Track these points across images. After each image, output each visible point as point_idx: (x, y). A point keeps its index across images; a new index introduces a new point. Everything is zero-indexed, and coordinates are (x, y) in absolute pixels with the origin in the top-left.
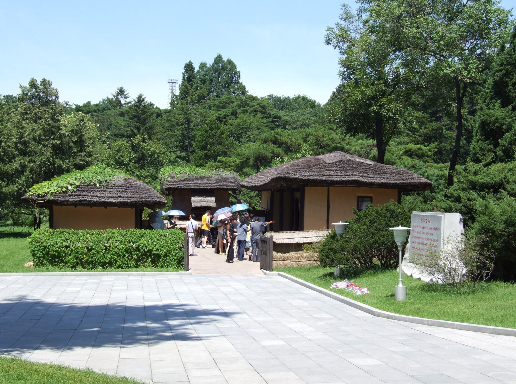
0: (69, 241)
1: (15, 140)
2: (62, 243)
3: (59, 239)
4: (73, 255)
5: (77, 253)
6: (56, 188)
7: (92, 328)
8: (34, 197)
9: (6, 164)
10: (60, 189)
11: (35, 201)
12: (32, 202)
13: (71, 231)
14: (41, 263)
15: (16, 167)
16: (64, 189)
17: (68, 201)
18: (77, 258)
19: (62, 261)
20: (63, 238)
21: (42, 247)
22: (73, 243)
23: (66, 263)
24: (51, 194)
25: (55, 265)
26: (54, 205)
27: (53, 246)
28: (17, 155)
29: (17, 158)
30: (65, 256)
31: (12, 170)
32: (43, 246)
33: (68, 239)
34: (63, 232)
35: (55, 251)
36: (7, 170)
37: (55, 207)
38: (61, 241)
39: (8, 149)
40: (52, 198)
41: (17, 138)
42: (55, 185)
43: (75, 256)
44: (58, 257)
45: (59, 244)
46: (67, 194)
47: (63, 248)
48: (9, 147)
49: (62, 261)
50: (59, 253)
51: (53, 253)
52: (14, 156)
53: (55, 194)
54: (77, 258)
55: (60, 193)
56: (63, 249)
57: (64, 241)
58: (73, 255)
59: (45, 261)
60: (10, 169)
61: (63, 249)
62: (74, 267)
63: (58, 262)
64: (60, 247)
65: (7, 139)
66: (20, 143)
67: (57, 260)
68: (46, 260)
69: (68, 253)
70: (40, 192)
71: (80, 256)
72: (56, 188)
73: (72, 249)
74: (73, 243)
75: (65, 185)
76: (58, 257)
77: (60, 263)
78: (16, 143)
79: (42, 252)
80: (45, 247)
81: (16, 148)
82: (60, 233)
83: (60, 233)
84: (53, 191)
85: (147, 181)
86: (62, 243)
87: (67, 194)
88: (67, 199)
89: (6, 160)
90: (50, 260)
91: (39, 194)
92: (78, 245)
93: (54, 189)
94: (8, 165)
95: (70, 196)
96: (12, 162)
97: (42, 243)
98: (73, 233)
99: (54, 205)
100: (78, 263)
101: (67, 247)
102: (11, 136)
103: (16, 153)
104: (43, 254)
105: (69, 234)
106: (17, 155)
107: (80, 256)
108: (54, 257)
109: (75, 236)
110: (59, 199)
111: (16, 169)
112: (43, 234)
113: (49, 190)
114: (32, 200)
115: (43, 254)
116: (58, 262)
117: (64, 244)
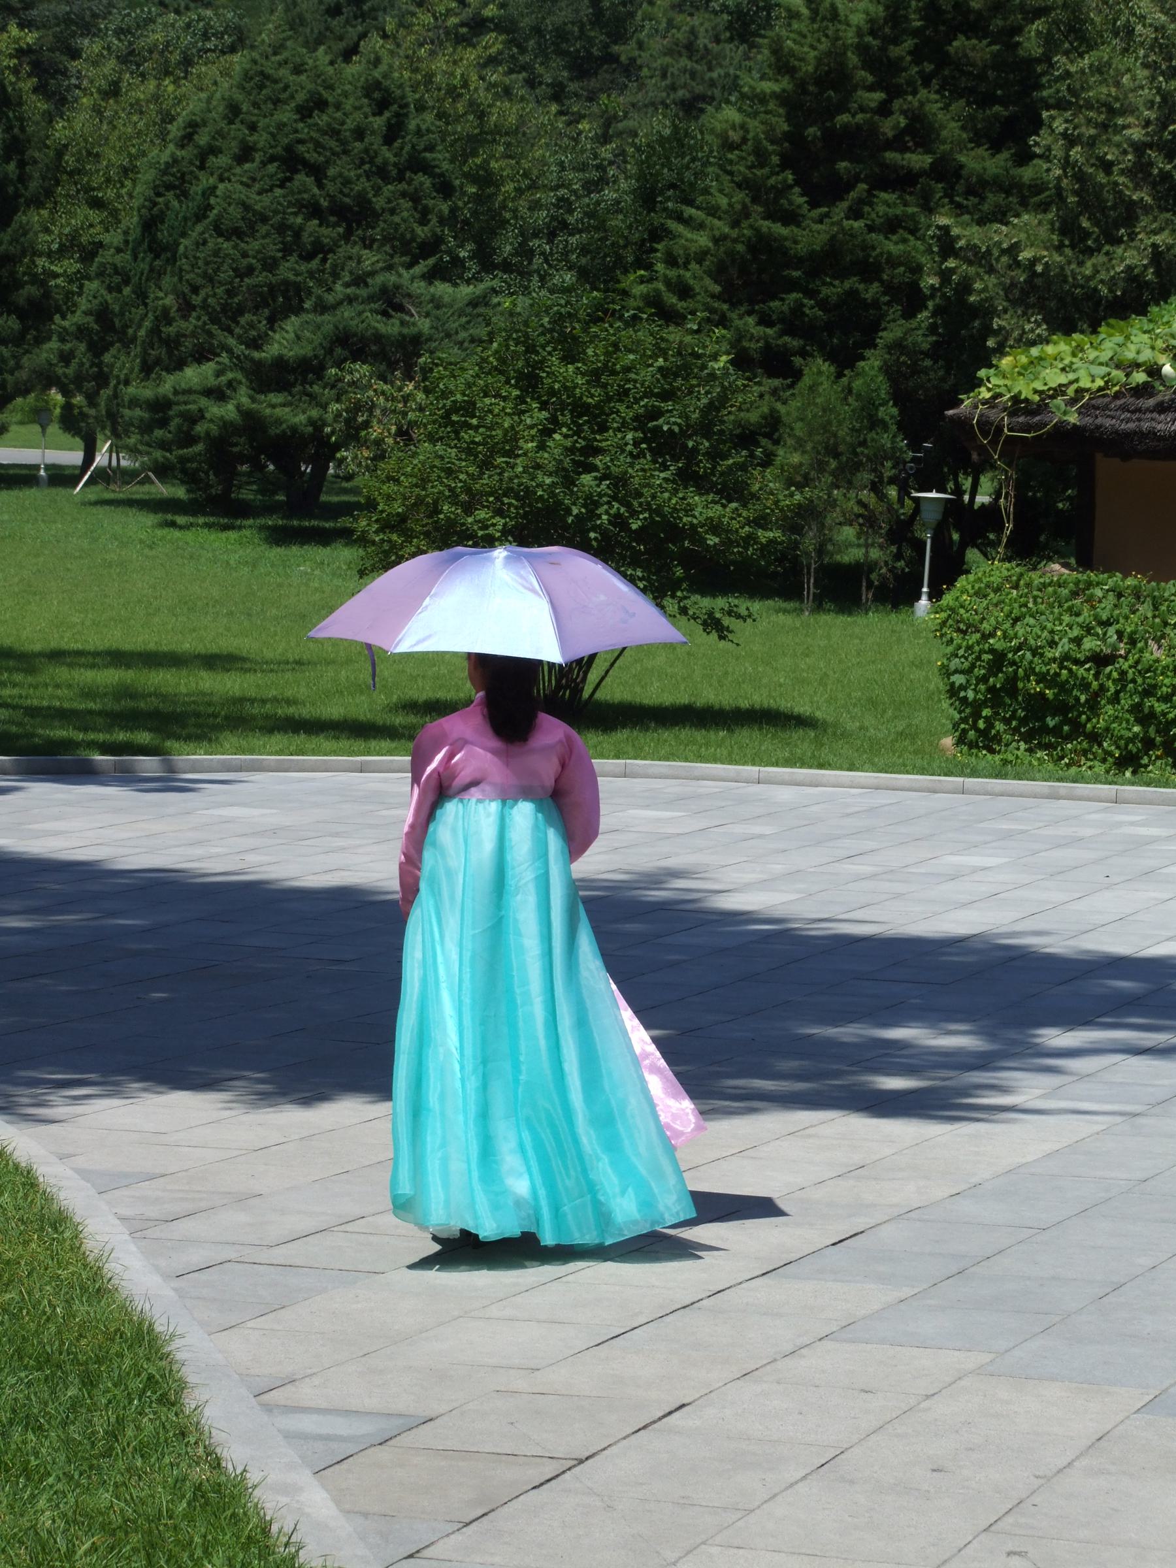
0: (1111, 631)
1: (1136, 134)
2: (1078, 641)
3: (1066, 618)
4: (1126, 702)
5: (1149, 692)
6: (1104, 370)
7: (834, 1023)
8: (994, 415)
9: (1090, 252)
10: (1118, 374)
11: (999, 429)
12: (985, 434)
13: (1130, 582)
14: (984, 733)
15: (1129, 268)
16: (1140, 377)
17: (1152, 433)
18: (1146, 718)
19: (1078, 729)
20: (1086, 616)
21: (986, 657)
22: (1133, 642)
23: (1095, 738)
24: (1073, 402)
25: (1041, 746)
26: (1099, 456)
27: (1035, 652)
28: (1147, 209)
29: (1144, 221)
30: (1093, 706)
31: (1112, 283)
32: (992, 651)
33: (1107, 624)
34: (1089, 584)
35: (1042, 678)
36: (1089, 279)
37: (1105, 465)
38: (1076, 632)
39: (1101, 178)
40: (1073, 418)
41: (1148, 123)
42: (1105, 356)
43: (1136, 709)
44: (1061, 708)
45: (1064, 646)
46: (1151, 402)
47: (1077, 662)
48: (1107, 167)
49: (1078, 729)
50: (1063, 687)
51: (1034, 687)
52: (1129, 213)
53: (1091, 402)
54: (1146, 718)
55: (1117, 396)
56: (1081, 672)
57: (1089, 630)
58: (1126, 702)
59: (1000, 726)
60: (1103, 275)
61: (1081, 672)
62: (1128, 762)
63: (1056, 731)
64: (1066, 657)
65: (1104, 127)
66: (1160, 146)
67: (1051, 722)
68: (1007, 721)
69: (1102, 688)
70: (1026, 389)
71: (1159, 707)
72: (1104, 370)
73: (1123, 673)
74: (1133, 642)
75: (1146, 355)
76: (1061, 708)
77: (1068, 738)
78: (1139, 148)
79: (984, 679)
80: (999, 659)
81: (1140, 172)
82: (1075, 594)
83: (1075, 594)
84: (1085, 383)
85: (695, 327)
86: (1078, 641)
87: (1151, 402)
88: (1145, 426)
89: (1087, 234)
90: (1023, 721)
91: (1016, 399)
92: (1155, 653)
93: (1089, 378)
94: (1100, 259)
95: (1161, 408)
96: (1119, 241)
97: (985, 637)
98: (1137, 595)
99: (1099, 456)
100: (1149, 744)
101: (1101, 660)
102: (1123, 112)
103: (1143, 195)
104: (991, 689)
105: (1120, 595)
106: (1147, 209)
107: (1159, 707)
108: (1037, 707)
109: (1145, 609)
110: (1108, 422)
111: (1132, 277)
112: (997, 590)
113: (1063, 379)
114: (984, 424)
115: (991, 689)
116: (1056, 731)
117: (1089, 644)
